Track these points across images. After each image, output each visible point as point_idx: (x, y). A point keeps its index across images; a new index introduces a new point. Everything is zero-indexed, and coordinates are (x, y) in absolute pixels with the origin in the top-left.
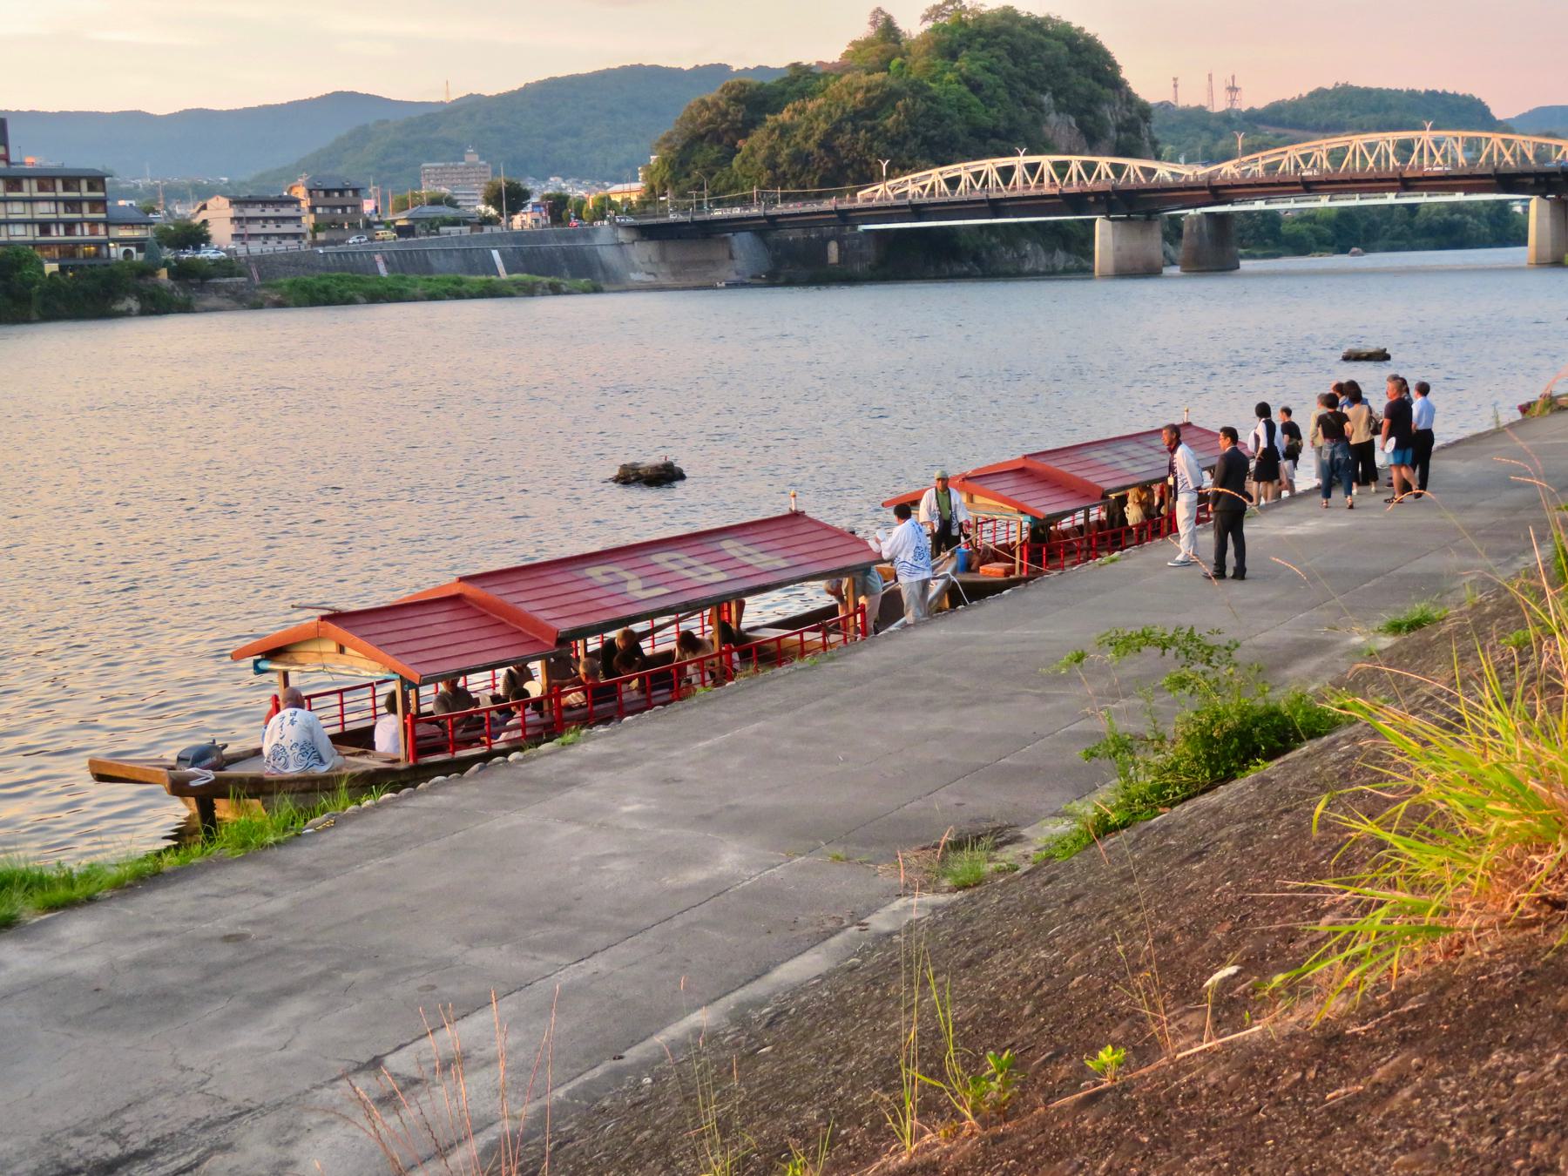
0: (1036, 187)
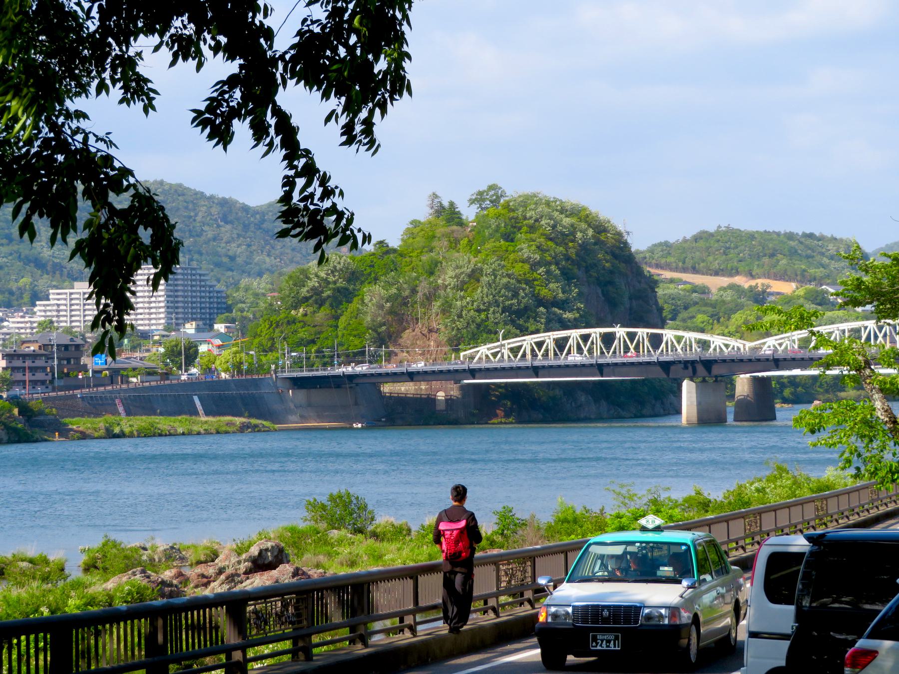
0: (564, 359)
